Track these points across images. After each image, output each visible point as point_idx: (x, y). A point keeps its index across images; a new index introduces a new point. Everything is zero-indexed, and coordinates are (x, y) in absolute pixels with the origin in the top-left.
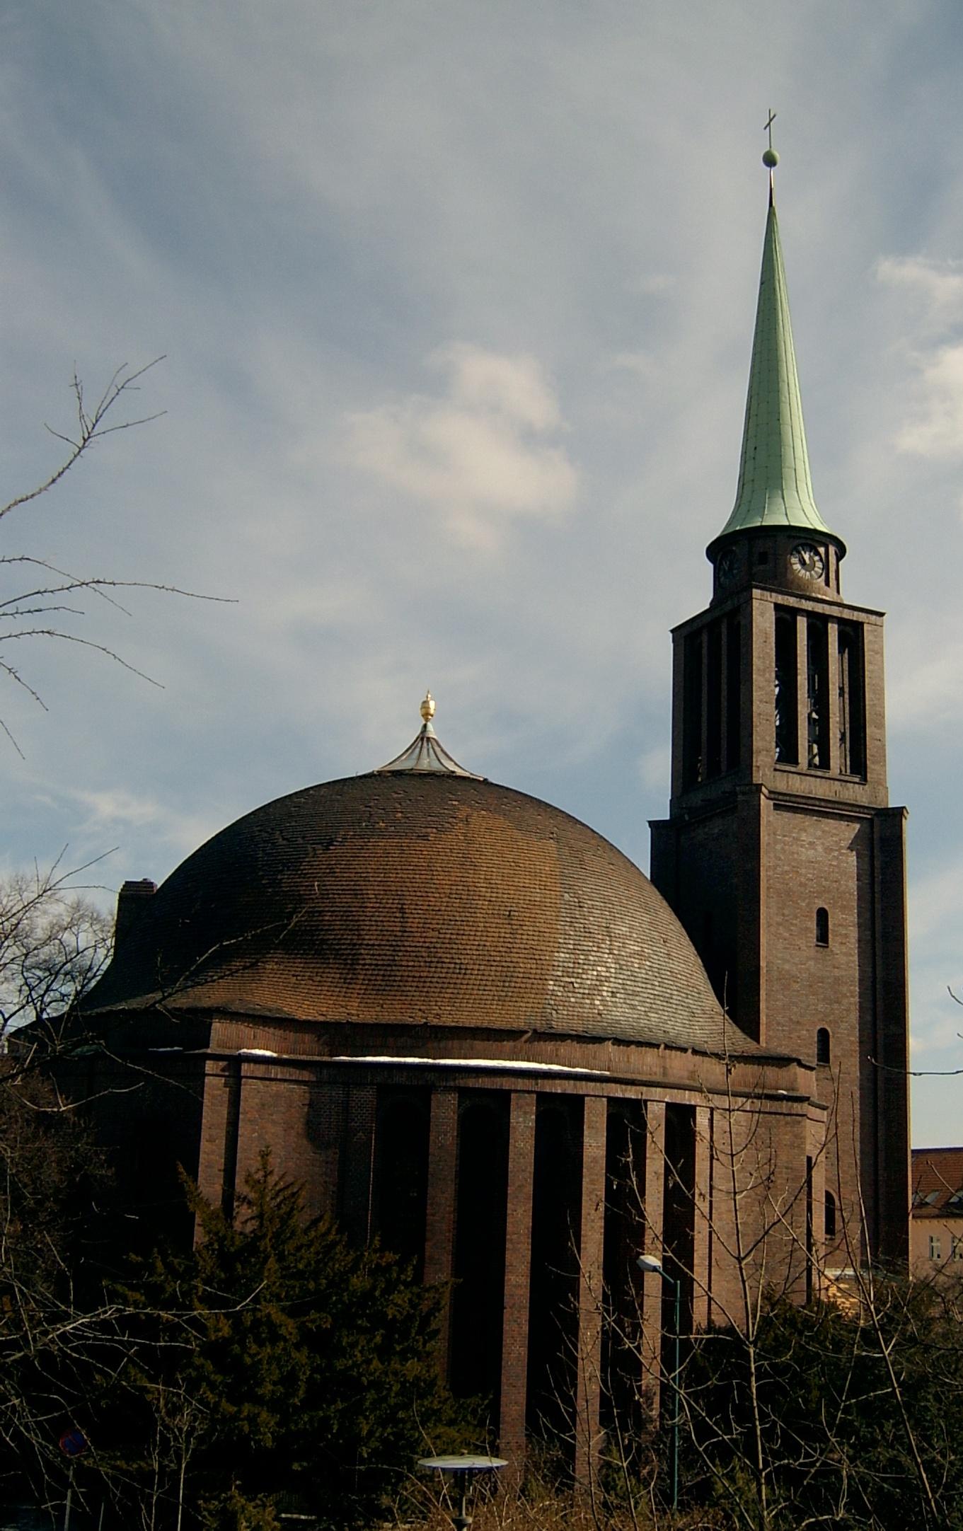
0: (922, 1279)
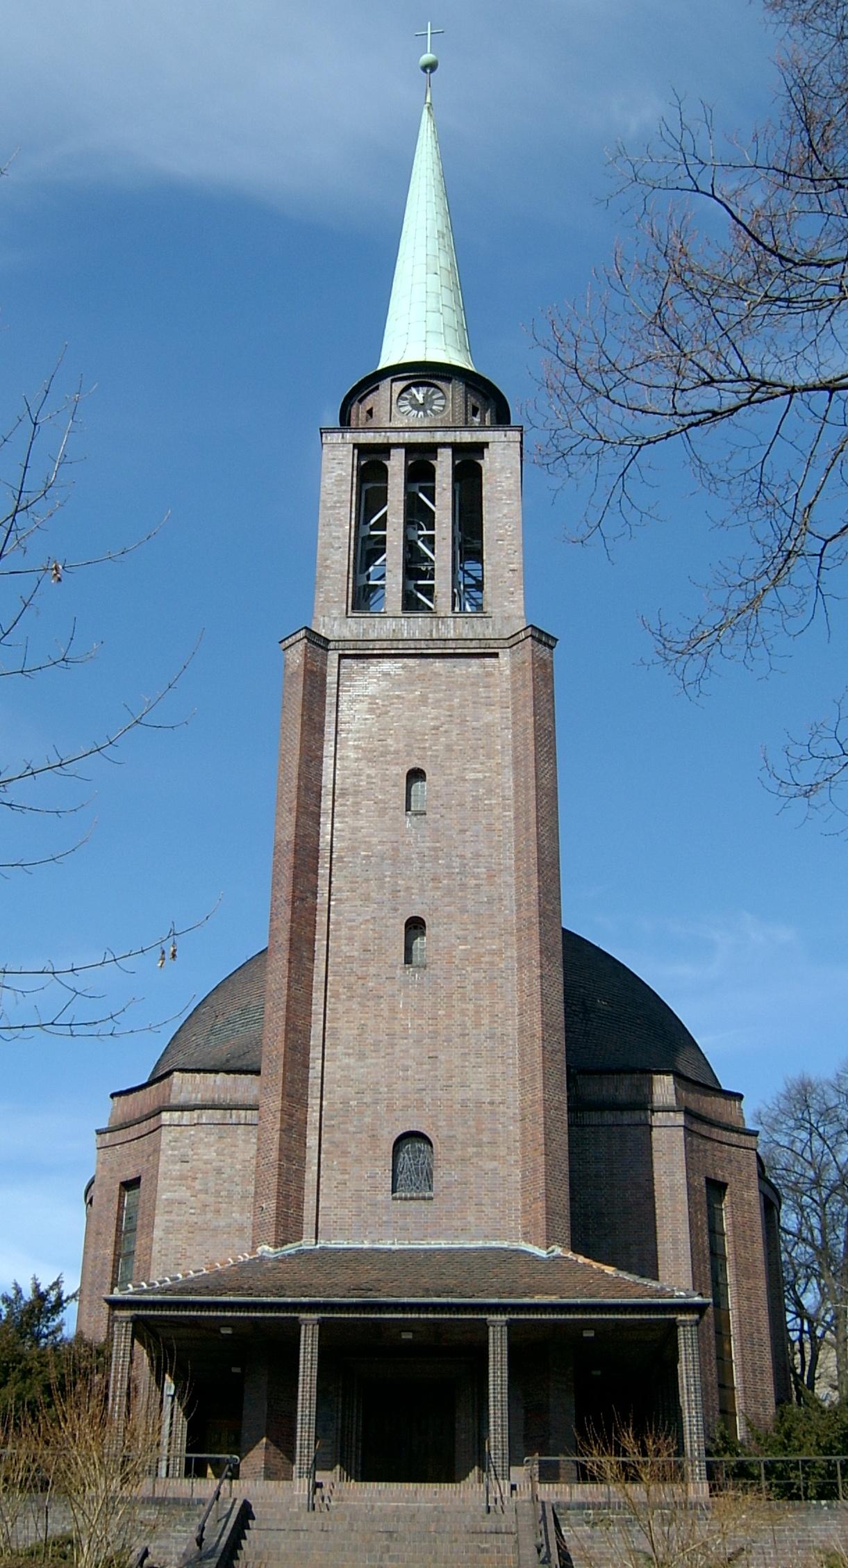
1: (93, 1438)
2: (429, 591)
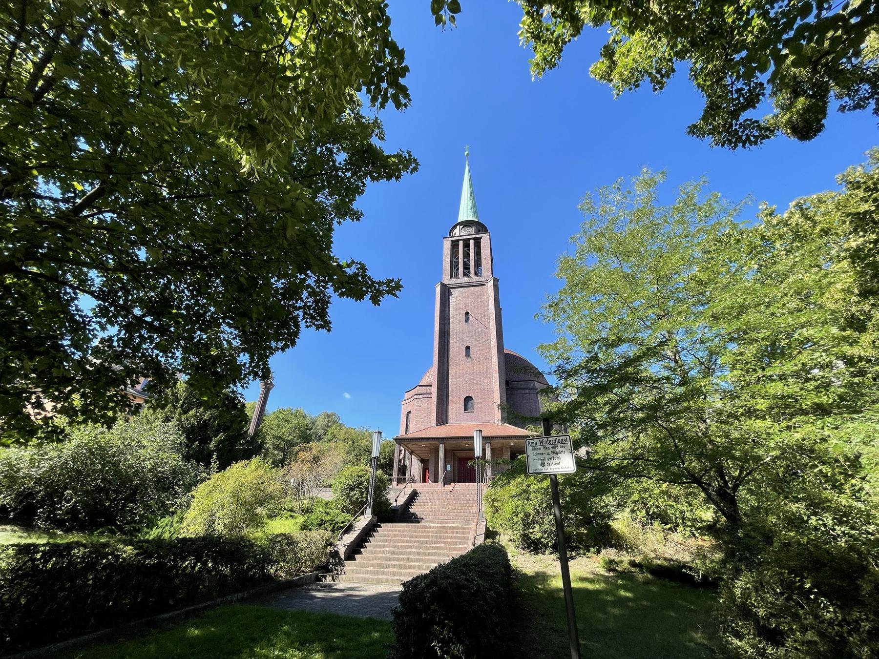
0: (852, 457)
2: (469, 272)
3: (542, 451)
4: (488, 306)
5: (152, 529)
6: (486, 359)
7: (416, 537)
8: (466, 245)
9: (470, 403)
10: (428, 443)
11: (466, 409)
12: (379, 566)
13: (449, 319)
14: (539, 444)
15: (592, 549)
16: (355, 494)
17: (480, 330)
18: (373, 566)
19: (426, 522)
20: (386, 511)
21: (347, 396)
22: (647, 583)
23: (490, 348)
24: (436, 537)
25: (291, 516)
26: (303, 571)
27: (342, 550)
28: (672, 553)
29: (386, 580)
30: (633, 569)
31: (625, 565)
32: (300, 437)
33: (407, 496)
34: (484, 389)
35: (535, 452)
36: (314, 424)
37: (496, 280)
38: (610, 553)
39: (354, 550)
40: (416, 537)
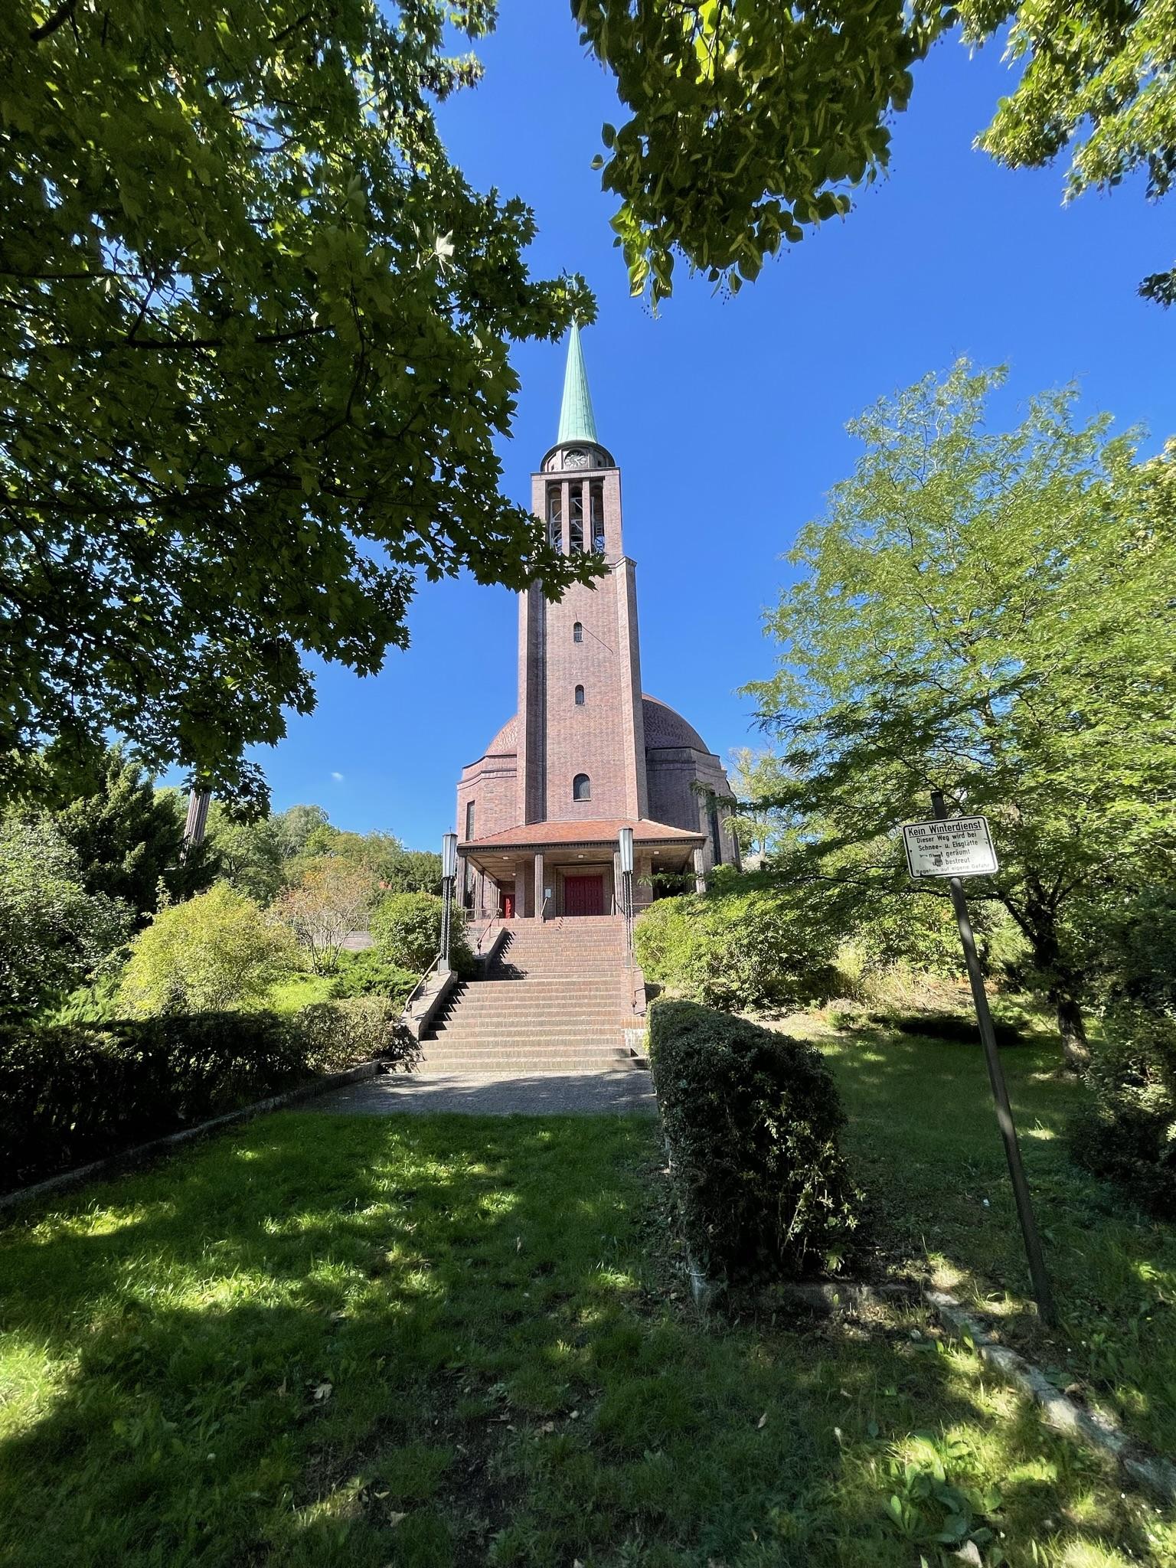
1: (898, 1405)
3: (936, 842)
4: (616, 613)
5: (58, 1010)
6: (612, 709)
7: (531, 998)
8: (576, 493)
9: (584, 785)
10: (513, 854)
11: (577, 796)
12: (479, 1045)
13: (544, 636)
14: (928, 832)
15: (813, 1002)
16: (418, 939)
17: (601, 656)
18: (469, 1045)
19: (534, 977)
20: (468, 964)
21: (337, 775)
22: (897, 1042)
23: (619, 690)
24: (564, 998)
25: (302, 978)
26: (356, 1060)
27: (415, 1030)
28: (925, 1000)
29: (498, 1065)
30: (873, 1025)
31: (863, 1021)
32: (258, 849)
33: (495, 939)
34: (609, 762)
35: (923, 844)
36: (280, 827)
37: (631, 564)
38: (840, 1006)
39: (433, 1024)
40: (531, 998)
